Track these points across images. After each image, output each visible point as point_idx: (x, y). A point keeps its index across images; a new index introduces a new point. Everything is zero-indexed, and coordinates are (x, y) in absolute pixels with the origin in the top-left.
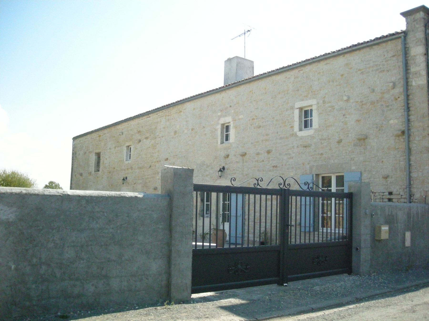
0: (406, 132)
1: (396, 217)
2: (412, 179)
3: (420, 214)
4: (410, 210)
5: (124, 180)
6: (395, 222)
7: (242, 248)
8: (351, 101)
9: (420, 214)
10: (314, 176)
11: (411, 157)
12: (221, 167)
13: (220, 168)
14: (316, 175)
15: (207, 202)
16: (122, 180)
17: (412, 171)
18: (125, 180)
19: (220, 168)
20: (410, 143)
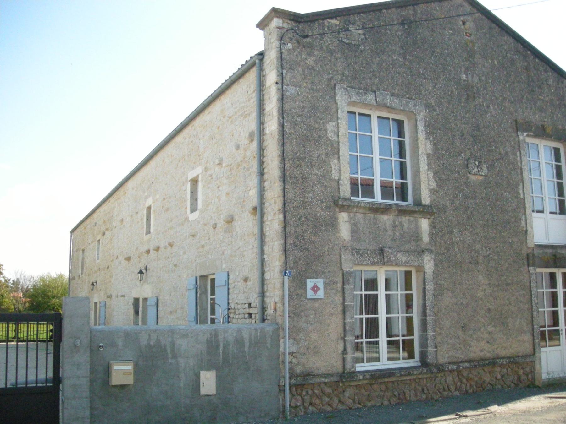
0: (258, 209)
1: (173, 350)
2: (265, 283)
3: (247, 345)
4: (216, 335)
5: (141, 272)
6: (170, 356)
7: (36, 387)
8: (224, 165)
9: (247, 345)
10: (198, 278)
11: (264, 248)
12: (143, 267)
13: (141, 269)
14: (201, 277)
15: (410, 317)
16: (139, 273)
17: (266, 270)
18: (143, 273)
19: (141, 269)
20: (264, 224)
